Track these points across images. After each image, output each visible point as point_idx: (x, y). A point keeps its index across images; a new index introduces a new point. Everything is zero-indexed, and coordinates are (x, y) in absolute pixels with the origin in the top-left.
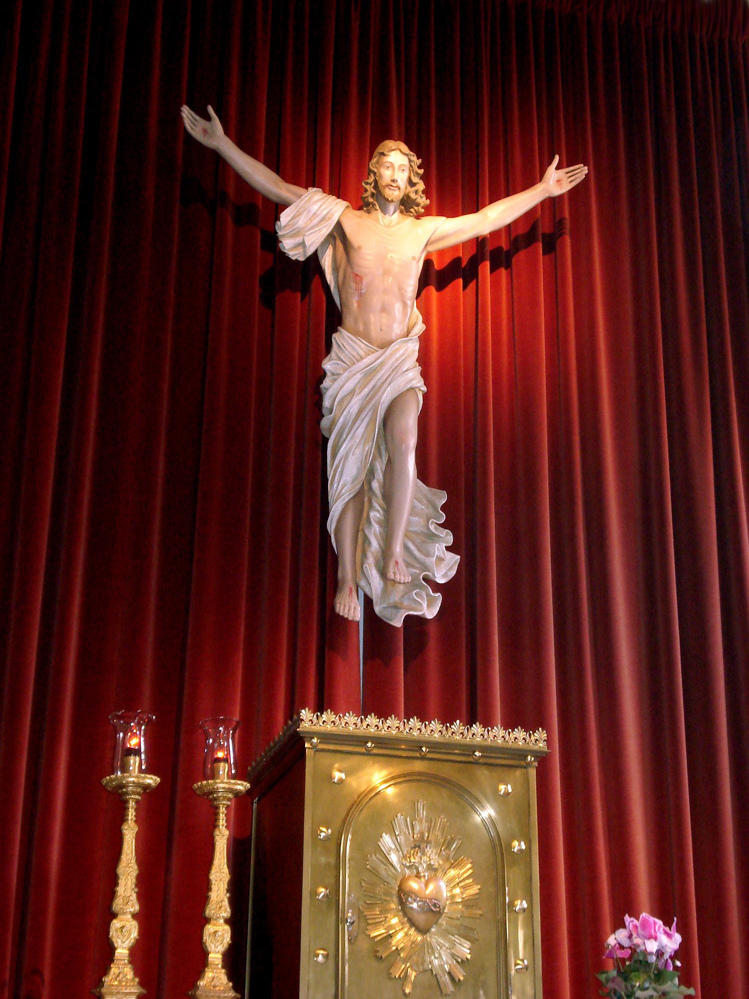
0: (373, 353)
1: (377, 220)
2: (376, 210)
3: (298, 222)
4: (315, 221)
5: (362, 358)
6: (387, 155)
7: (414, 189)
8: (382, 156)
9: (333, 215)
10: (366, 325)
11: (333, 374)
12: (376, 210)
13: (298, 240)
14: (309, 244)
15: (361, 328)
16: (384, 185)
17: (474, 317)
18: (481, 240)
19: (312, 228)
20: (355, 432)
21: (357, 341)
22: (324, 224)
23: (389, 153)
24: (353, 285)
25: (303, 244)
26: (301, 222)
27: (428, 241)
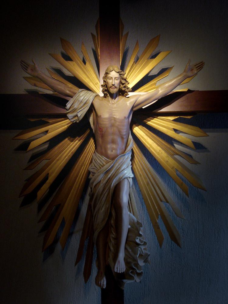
0: (109, 162)
1: (109, 101)
2: (108, 97)
3: (74, 106)
4: (82, 105)
5: (104, 165)
6: (109, 74)
7: (123, 86)
8: (107, 74)
9: (90, 100)
10: (106, 150)
11: (93, 173)
12: (108, 97)
13: (75, 114)
14: (80, 115)
15: (103, 151)
16: (109, 86)
17: (150, 102)
18: (151, 76)
19: (81, 108)
20: (101, 200)
21: (102, 158)
22: (86, 105)
23: (110, 73)
24: (99, 132)
25: (77, 116)
26: (76, 106)
27: (133, 106)
